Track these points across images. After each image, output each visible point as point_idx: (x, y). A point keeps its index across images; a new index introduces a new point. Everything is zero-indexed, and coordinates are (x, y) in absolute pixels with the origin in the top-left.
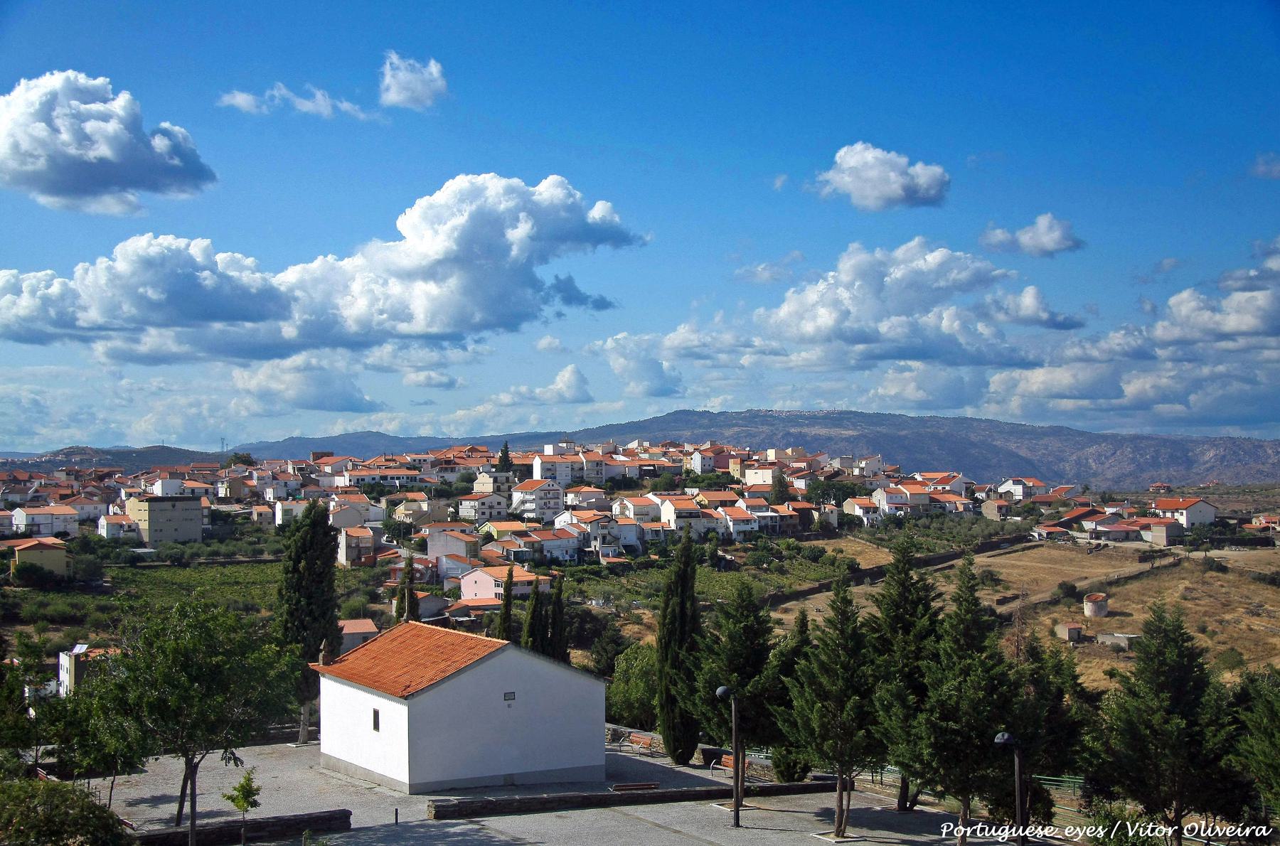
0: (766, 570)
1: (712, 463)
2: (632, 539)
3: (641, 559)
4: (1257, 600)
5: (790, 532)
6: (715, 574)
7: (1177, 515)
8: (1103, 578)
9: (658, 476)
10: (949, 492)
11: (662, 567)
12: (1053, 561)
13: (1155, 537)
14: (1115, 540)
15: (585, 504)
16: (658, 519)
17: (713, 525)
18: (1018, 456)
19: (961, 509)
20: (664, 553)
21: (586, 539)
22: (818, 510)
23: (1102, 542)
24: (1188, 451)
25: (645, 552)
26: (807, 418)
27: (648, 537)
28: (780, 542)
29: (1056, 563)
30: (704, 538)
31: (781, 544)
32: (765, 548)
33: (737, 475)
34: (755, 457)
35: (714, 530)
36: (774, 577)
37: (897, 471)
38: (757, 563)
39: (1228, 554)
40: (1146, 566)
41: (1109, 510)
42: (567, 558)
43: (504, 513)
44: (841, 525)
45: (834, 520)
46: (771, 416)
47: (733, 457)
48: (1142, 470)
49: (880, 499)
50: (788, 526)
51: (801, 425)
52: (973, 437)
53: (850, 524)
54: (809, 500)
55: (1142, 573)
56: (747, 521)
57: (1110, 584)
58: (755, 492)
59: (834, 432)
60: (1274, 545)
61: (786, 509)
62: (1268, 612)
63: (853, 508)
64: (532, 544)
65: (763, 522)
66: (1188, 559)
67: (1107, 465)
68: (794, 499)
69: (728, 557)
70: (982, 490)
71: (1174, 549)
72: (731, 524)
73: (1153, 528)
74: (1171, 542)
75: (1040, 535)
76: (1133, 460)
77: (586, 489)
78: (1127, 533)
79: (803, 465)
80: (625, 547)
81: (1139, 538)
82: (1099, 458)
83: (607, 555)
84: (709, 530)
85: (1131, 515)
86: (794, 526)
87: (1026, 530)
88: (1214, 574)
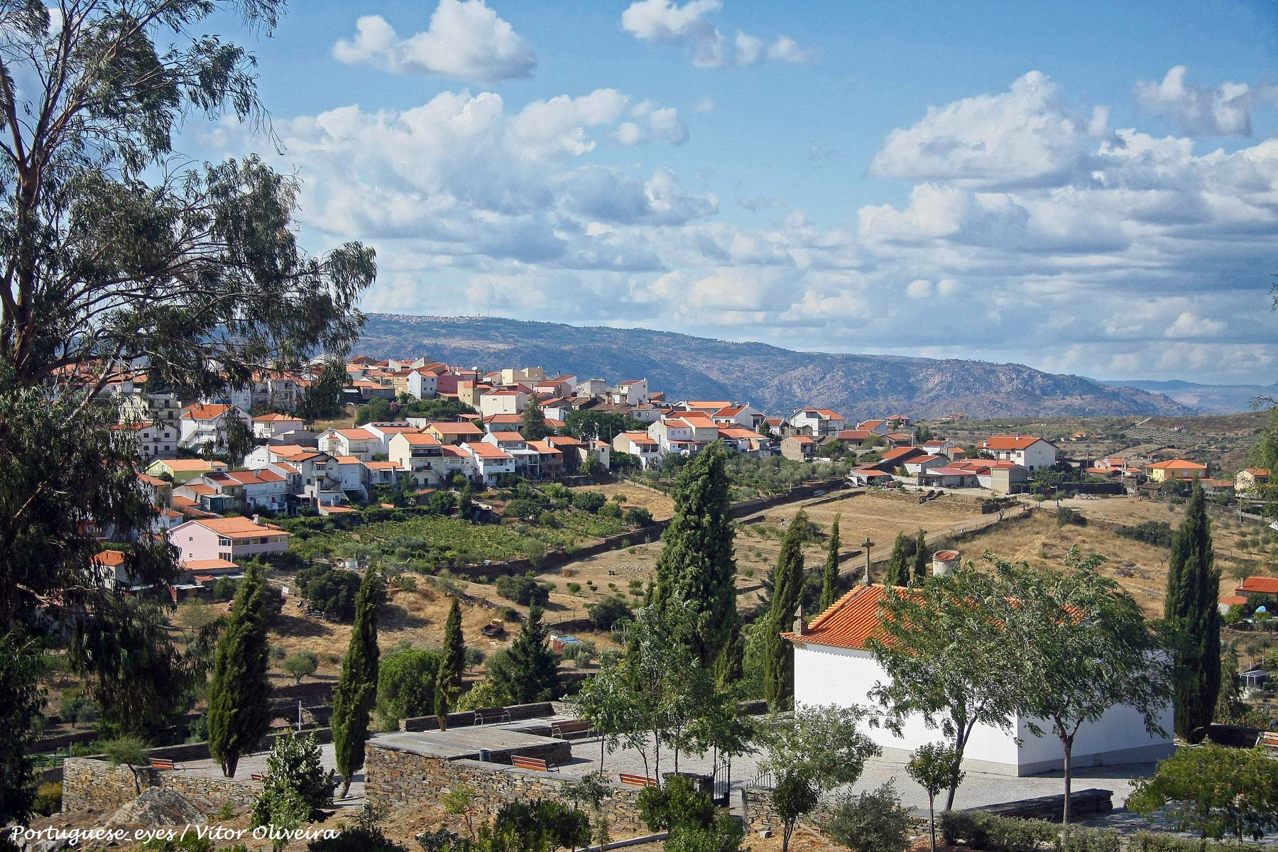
0: (533, 523)
1: (435, 386)
2: (354, 482)
3: (371, 509)
4: (1126, 558)
5: (553, 475)
6: (470, 528)
7: (1013, 457)
8: (947, 532)
9: (366, 401)
10: (736, 426)
11: (401, 519)
12: (878, 511)
13: (997, 483)
14: (949, 486)
15: (281, 438)
16: (385, 457)
17: (458, 466)
18: (710, 380)
19: (756, 447)
20: (400, 501)
21: (297, 483)
22: (586, 447)
23: (935, 488)
24: (909, 376)
25: (374, 500)
26: (443, 327)
27: (376, 481)
28: (543, 486)
29: (885, 514)
30: (448, 481)
31: (548, 489)
32: (528, 495)
33: (469, 402)
34: (486, 379)
35: (459, 471)
36: (546, 531)
37: (662, 398)
38: (522, 515)
39: (1078, 502)
40: (993, 518)
41: (931, 451)
42: (276, 507)
43: (173, 448)
44: (614, 466)
45: (605, 460)
46: (397, 323)
47: (462, 378)
48: (856, 399)
49: (658, 433)
50: (550, 467)
51: (437, 336)
52: (654, 356)
53: (624, 465)
54: (567, 433)
55: (989, 526)
56: (501, 461)
57: (957, 539)
58: (500, 426)
59: (479, 345)
60: (1125, 493)
61: (545, 446)
62: (1142, 572)
63: (627, 444)
64: (231, 489)
65: (520, 463)
66: (1039, 508)
67: (814, 392)
68: (550, 433)
69: (484, 506)
70: (776, 424)
71: (1022, 498)
72: (481, 465)
73: (994, 472)
74: (1015, 489)
75: (859, 480)
76: (845, 387)
77: (279, 417)
78: (962, 478)
79: (551, 390)
80: (347, 493)
81: (975, 484)
82: (805, 382)
83: (327, 504)
84: (453, 473)
85: (958, 456)
86: (557, 467)
87: (843, 473)
88: (1072, 527)
